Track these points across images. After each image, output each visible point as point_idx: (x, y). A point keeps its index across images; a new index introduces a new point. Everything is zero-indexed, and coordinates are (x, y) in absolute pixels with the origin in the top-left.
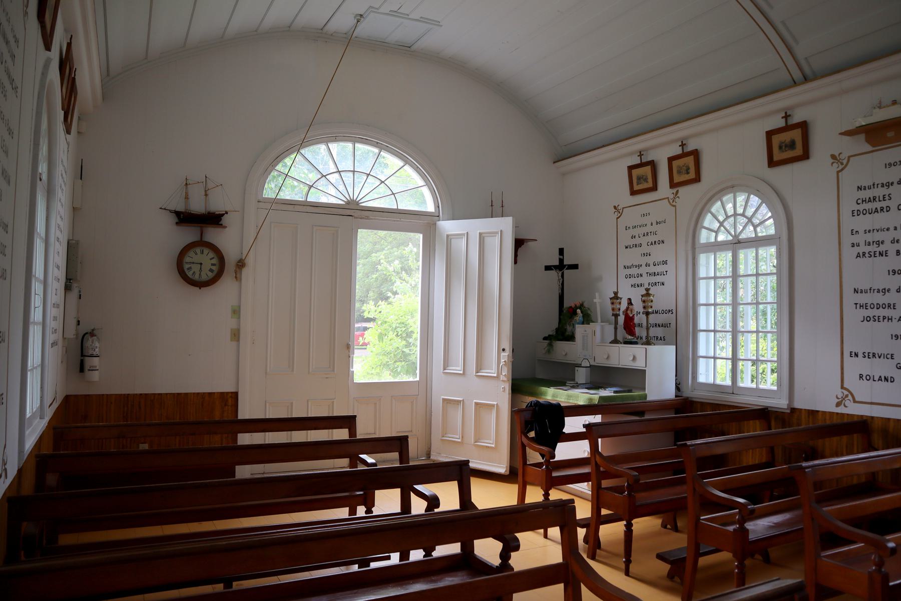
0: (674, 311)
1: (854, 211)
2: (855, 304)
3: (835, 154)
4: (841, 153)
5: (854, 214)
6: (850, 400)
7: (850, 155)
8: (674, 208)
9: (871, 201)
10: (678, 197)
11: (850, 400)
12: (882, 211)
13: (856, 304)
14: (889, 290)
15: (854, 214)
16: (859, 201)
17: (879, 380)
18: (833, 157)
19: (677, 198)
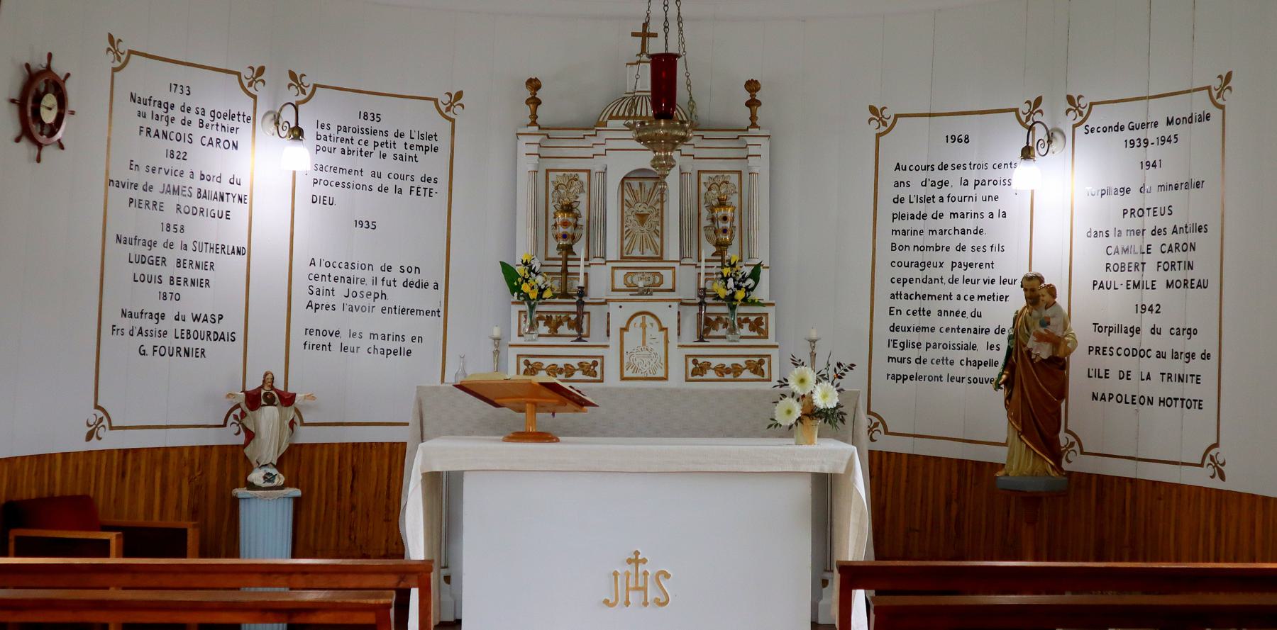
0: (694, 358)
1: (1130, 281)
2: (1161, 374)
3: (877, 107)
4: (885, 108)
5: (1129, 287)
6: (246, 78)
7: (223, 428)
8: (222, 424)
9: (1172, 251)
10: (89, 426)
11: (246, 78)
12: (178, 211)
13: (1163, 374)
14: (1138, 330)
15: (1129, 287)
16: (1110, 251)
17: (1147, 379)
18: (873, 110)
19: (91, 423)
